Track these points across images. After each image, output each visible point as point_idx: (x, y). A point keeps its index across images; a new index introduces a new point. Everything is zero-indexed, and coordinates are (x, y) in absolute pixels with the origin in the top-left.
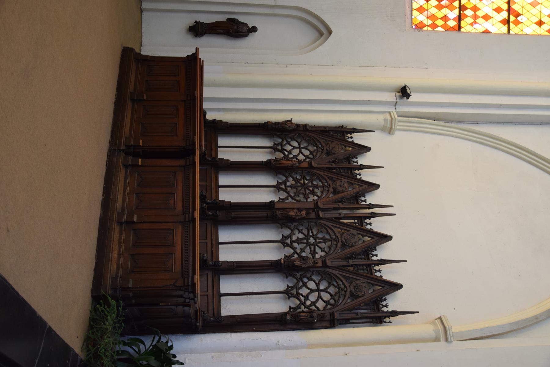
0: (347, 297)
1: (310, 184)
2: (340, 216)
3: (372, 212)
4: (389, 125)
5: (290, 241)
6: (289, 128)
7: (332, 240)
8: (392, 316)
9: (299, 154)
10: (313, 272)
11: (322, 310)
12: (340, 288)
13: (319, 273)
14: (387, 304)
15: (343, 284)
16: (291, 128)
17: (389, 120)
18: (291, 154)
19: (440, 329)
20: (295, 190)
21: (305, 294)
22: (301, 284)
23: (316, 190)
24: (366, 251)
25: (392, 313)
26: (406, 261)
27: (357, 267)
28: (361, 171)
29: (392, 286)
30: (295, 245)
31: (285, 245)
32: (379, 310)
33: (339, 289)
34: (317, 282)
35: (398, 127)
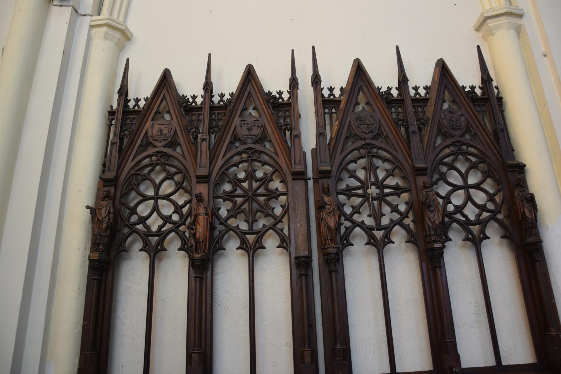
0: (262, 149)
1: (255, 185)
2: (206, 140)
3: (118, 93)
4: (118, 35)
5: (377, 230)
6: (111, 214)
7: (250, 160)
8: (212, 92)
9: (172, 202)
10: (121, 203)
11: (191, 196)
12: (157, 162)
13: (125, 195)
14: (134, 99)
15: (150, 156)
16: (112, 210)
17: (108, 31)
18: (171, 216)
19: (506, 21)
20: (242, 215)
21: (160, 222)
22: (140, 227)
23: (259, 174)
24: (185, 111)
25: (207, 89)
26: (397, 48)
27: (214, 127)
28: (131, 96)
29: (250, 81)
30: (385, 221)
31: (387, 240)
32: (199, 109)
33: (158, 164)
34: (140, 198)
35: (121, 19)
